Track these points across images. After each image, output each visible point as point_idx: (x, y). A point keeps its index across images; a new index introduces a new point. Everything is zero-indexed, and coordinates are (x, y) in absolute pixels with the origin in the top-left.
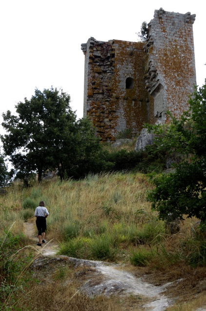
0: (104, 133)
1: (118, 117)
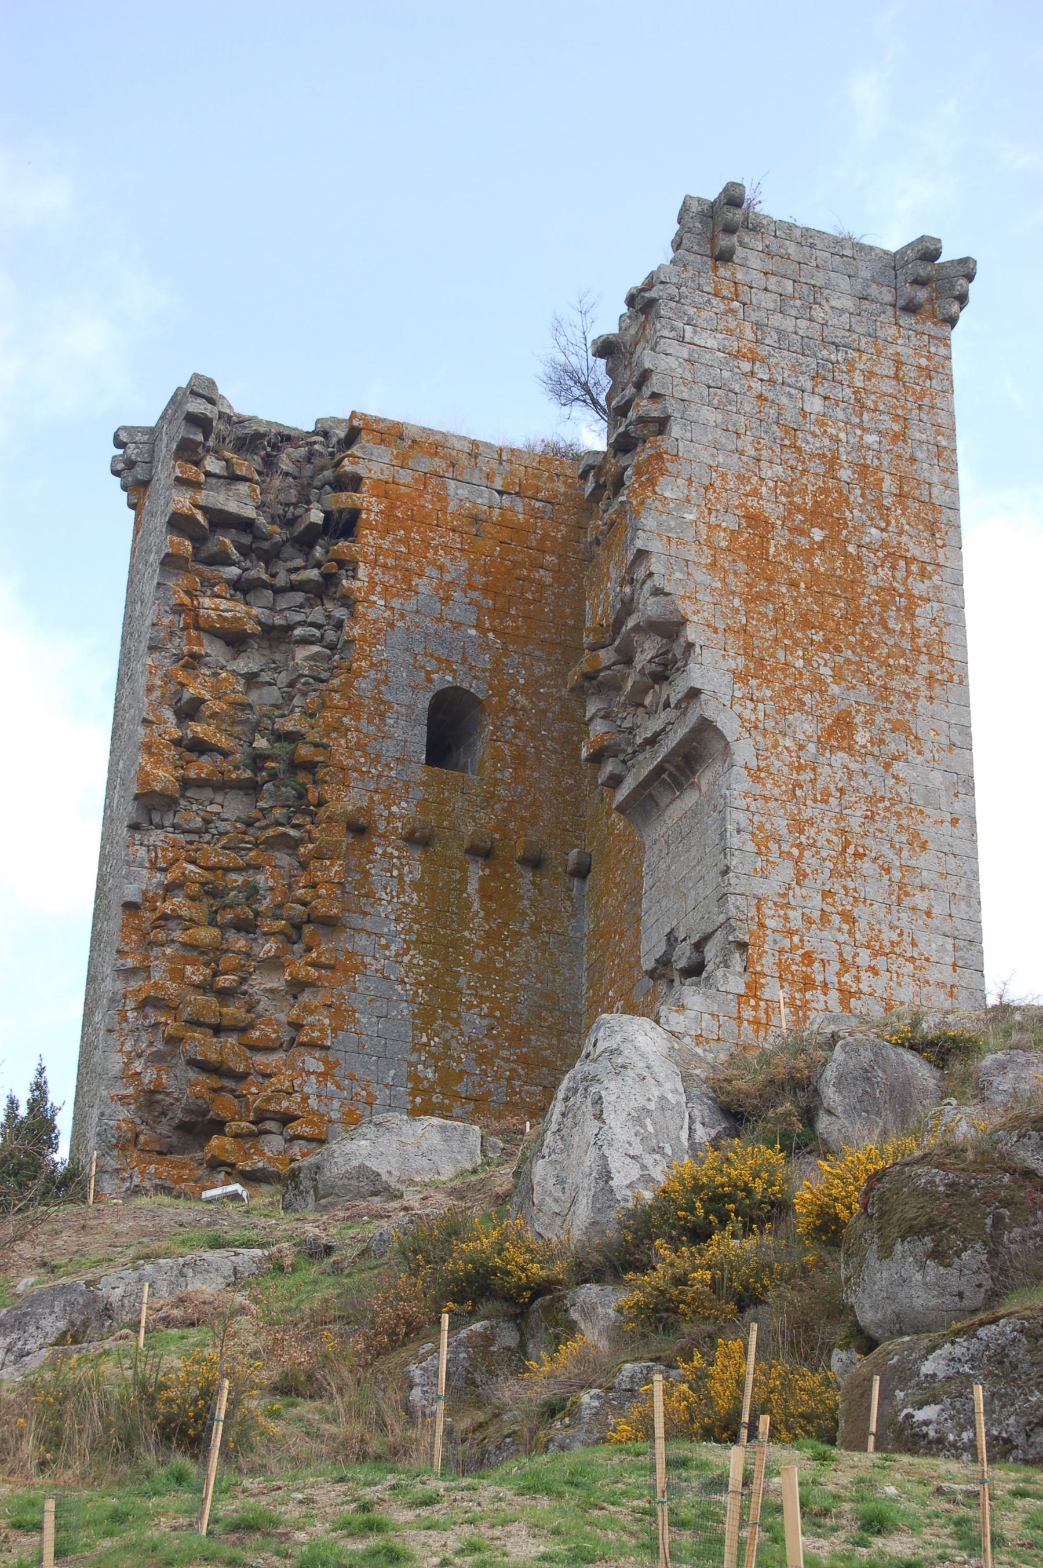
0: (242, 1077)
1: (360, 968)
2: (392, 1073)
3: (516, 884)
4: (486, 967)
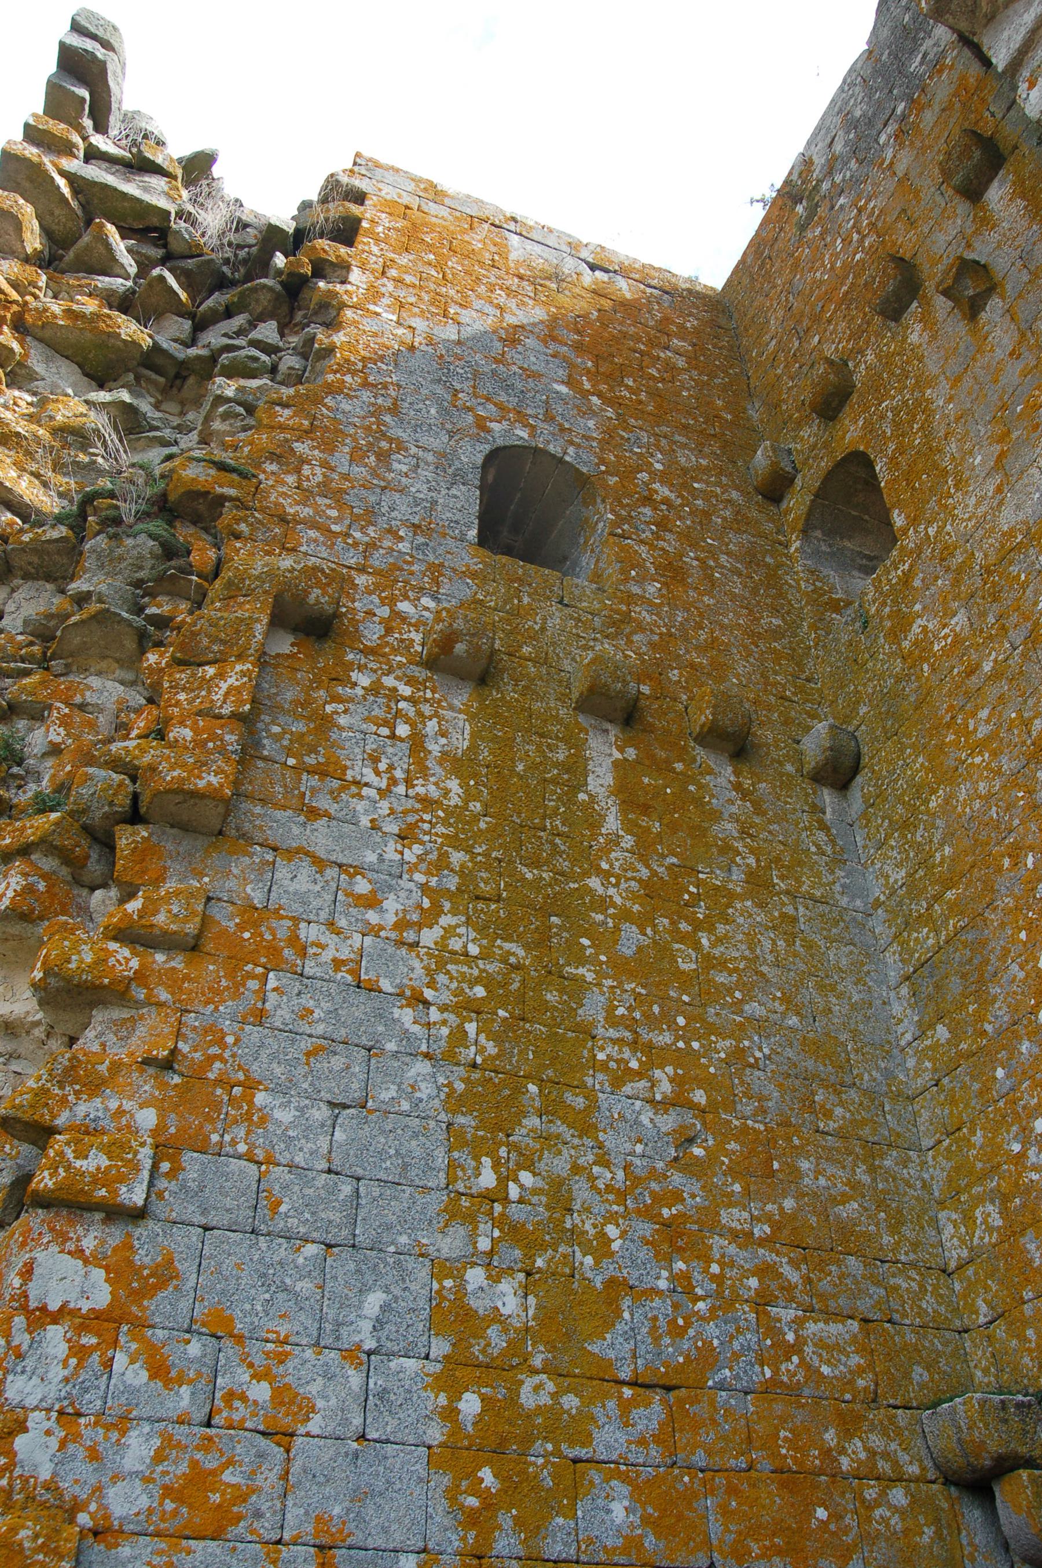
1: (285, 955)
2: (374, 1301)
3: (701, 787)
4: (651, 967)
